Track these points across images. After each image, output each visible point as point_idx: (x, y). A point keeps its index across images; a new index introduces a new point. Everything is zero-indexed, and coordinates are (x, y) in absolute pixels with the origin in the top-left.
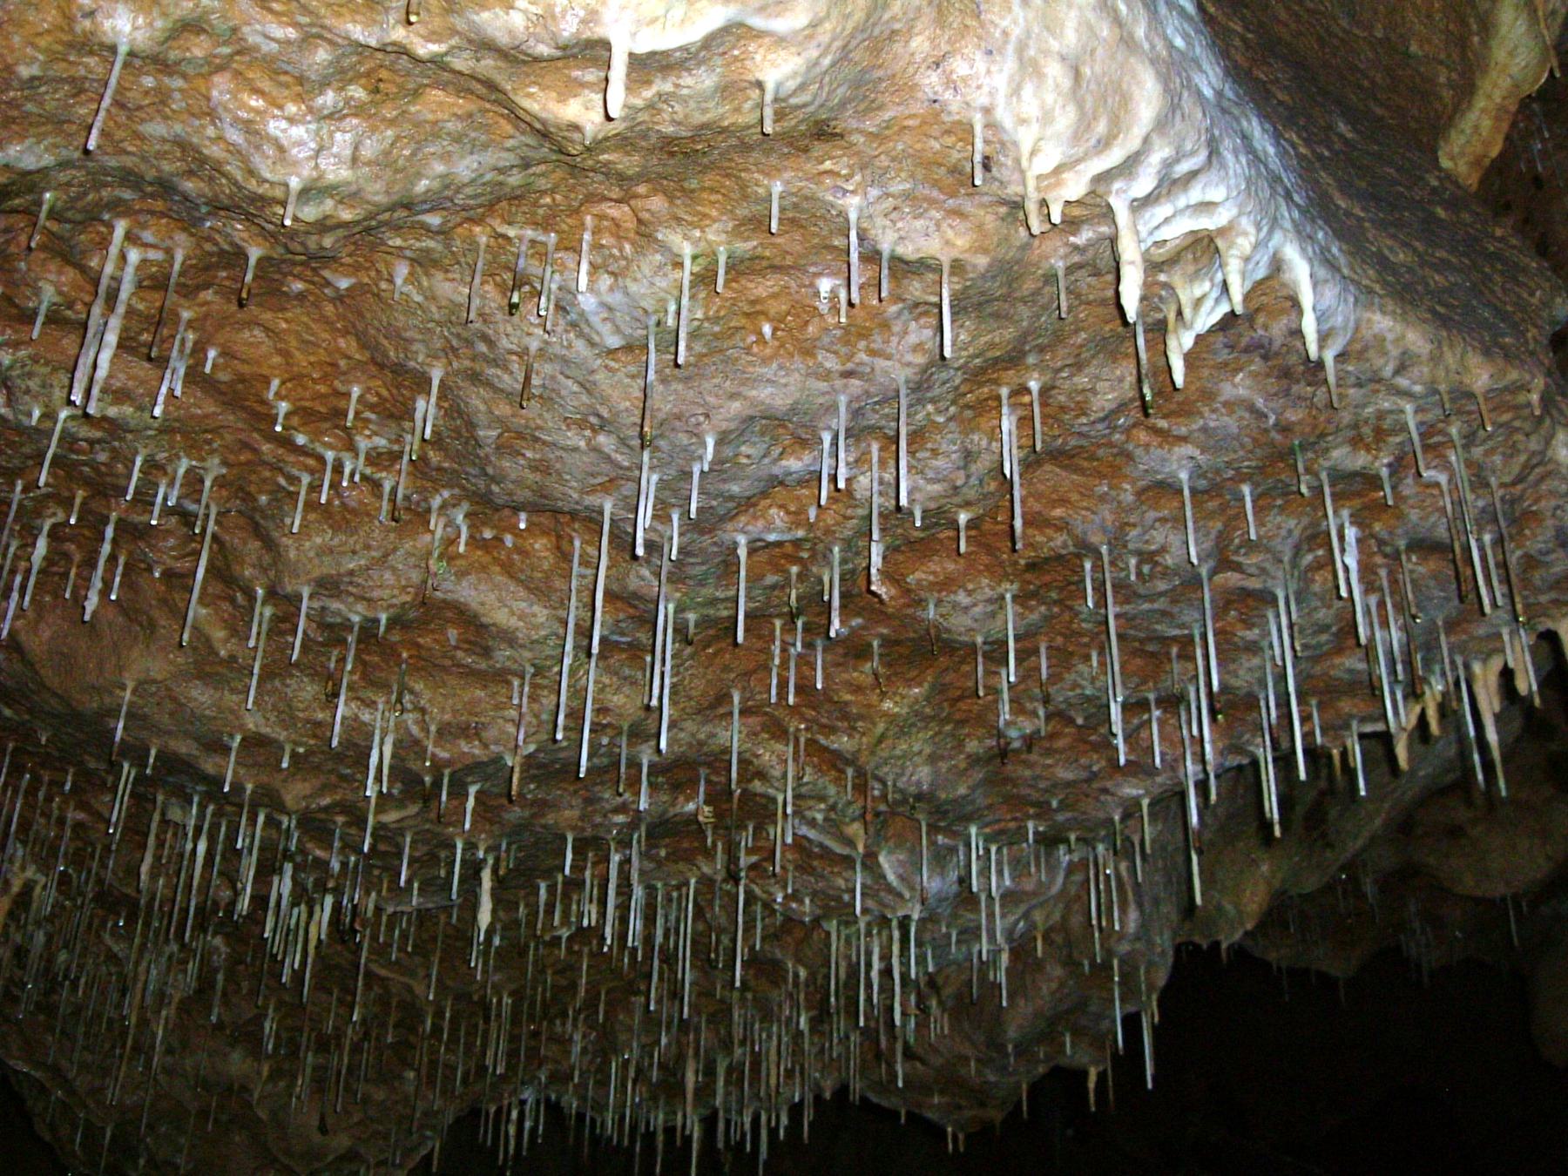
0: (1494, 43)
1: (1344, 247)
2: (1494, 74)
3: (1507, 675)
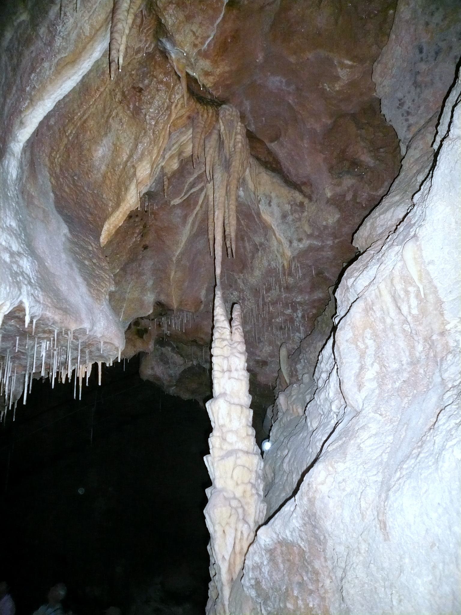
0: (128, 194)
1: (43, 294)
2: (126, 202)
3: (67, 375)
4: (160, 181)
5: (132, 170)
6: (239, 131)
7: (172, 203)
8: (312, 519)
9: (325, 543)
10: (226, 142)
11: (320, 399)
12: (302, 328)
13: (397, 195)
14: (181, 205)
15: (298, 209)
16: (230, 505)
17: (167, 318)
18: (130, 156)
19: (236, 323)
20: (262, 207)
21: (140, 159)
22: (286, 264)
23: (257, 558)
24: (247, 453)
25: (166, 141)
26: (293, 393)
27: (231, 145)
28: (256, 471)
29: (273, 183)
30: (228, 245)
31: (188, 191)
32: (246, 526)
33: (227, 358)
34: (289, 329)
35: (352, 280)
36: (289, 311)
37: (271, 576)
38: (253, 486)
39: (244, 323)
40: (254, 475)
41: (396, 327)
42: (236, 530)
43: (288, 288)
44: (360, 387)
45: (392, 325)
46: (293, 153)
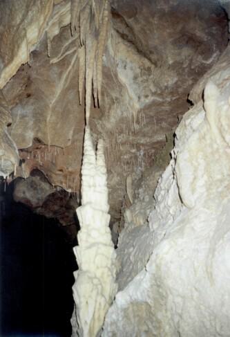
4: (44, 44)
5: (24, 32)
6: (106, 7)
7: (51, 62)
8: (158, 283)
9: (166, 298)
10: (96, 16)
11: (160, 208)
12: (143, 163)
13: (224, 61)
14: (58, 64)
15: (146, 72)
16: (92, 283)
17: (42, 152)
18: (22, 21)
19: (100, 152)
20: (120, 71)
21: (30, 24)
22: (135, 114)
23: (114, 316)
24: (106, 245)
25: (51, 11)
26: (137, 209)
27: (100, 18)
28: (112, 259)
29: (128, 51)
30: (95, 96)
31: (64, 53)
32: (103, 298)
33: (93, 177)
34: (133, 164)
35: (189, 120)
36: (134, 151)
37: (124, 329)
38: (109, 269)
39: (106, 153)
40: (110, 262)
41: (221, 151)
42: (96, 301)
43: (135, 134)
44: (193, 191)
45: (218, 149)
46: (145, 28)
